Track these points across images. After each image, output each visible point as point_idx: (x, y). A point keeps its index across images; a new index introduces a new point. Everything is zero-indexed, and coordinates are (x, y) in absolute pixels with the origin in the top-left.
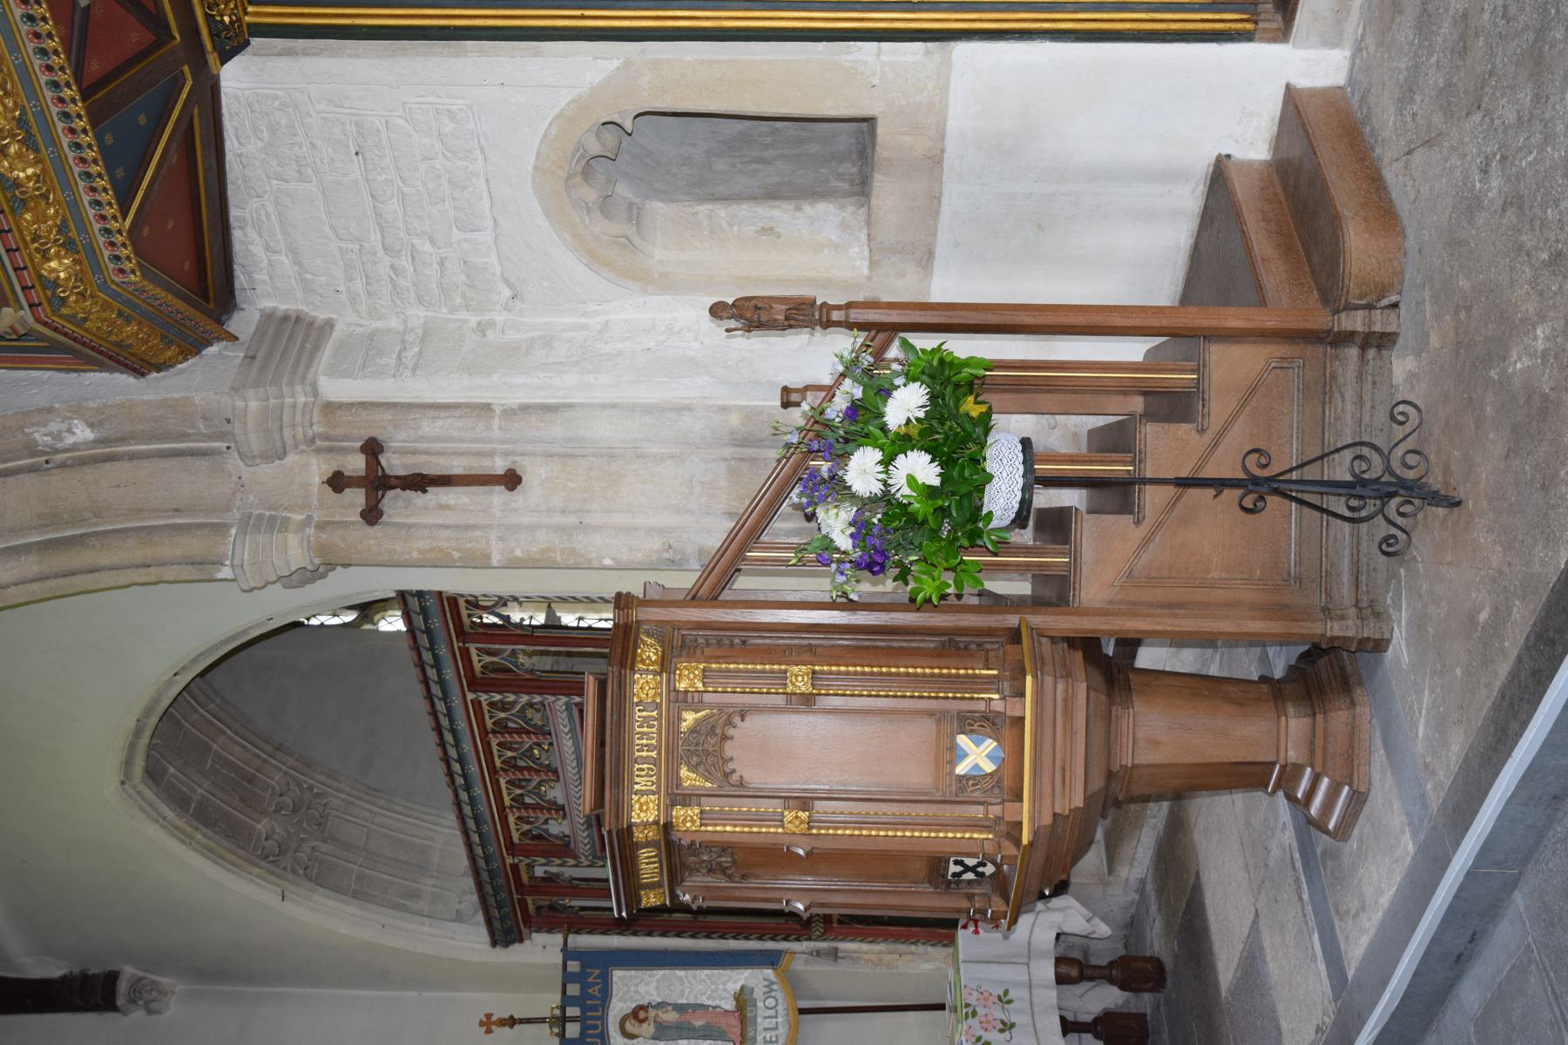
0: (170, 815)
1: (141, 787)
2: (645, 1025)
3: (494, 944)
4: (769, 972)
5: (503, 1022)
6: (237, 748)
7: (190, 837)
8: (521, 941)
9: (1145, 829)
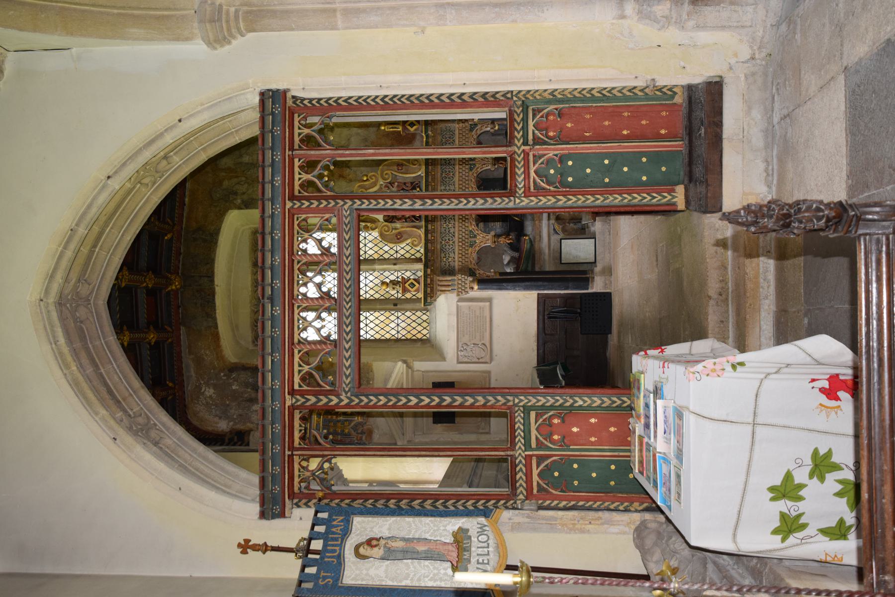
0: (62, 340)
1: (52, 308)
2: (376, 549)
3: (263, 515)
4: (482, 520)
5: (256, 548)
6: (116, 377)
7: (67, 366)
8: (282, 515)
9: (763, 314)
